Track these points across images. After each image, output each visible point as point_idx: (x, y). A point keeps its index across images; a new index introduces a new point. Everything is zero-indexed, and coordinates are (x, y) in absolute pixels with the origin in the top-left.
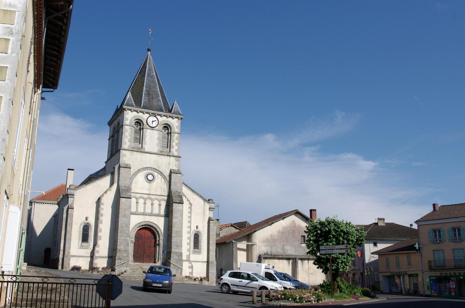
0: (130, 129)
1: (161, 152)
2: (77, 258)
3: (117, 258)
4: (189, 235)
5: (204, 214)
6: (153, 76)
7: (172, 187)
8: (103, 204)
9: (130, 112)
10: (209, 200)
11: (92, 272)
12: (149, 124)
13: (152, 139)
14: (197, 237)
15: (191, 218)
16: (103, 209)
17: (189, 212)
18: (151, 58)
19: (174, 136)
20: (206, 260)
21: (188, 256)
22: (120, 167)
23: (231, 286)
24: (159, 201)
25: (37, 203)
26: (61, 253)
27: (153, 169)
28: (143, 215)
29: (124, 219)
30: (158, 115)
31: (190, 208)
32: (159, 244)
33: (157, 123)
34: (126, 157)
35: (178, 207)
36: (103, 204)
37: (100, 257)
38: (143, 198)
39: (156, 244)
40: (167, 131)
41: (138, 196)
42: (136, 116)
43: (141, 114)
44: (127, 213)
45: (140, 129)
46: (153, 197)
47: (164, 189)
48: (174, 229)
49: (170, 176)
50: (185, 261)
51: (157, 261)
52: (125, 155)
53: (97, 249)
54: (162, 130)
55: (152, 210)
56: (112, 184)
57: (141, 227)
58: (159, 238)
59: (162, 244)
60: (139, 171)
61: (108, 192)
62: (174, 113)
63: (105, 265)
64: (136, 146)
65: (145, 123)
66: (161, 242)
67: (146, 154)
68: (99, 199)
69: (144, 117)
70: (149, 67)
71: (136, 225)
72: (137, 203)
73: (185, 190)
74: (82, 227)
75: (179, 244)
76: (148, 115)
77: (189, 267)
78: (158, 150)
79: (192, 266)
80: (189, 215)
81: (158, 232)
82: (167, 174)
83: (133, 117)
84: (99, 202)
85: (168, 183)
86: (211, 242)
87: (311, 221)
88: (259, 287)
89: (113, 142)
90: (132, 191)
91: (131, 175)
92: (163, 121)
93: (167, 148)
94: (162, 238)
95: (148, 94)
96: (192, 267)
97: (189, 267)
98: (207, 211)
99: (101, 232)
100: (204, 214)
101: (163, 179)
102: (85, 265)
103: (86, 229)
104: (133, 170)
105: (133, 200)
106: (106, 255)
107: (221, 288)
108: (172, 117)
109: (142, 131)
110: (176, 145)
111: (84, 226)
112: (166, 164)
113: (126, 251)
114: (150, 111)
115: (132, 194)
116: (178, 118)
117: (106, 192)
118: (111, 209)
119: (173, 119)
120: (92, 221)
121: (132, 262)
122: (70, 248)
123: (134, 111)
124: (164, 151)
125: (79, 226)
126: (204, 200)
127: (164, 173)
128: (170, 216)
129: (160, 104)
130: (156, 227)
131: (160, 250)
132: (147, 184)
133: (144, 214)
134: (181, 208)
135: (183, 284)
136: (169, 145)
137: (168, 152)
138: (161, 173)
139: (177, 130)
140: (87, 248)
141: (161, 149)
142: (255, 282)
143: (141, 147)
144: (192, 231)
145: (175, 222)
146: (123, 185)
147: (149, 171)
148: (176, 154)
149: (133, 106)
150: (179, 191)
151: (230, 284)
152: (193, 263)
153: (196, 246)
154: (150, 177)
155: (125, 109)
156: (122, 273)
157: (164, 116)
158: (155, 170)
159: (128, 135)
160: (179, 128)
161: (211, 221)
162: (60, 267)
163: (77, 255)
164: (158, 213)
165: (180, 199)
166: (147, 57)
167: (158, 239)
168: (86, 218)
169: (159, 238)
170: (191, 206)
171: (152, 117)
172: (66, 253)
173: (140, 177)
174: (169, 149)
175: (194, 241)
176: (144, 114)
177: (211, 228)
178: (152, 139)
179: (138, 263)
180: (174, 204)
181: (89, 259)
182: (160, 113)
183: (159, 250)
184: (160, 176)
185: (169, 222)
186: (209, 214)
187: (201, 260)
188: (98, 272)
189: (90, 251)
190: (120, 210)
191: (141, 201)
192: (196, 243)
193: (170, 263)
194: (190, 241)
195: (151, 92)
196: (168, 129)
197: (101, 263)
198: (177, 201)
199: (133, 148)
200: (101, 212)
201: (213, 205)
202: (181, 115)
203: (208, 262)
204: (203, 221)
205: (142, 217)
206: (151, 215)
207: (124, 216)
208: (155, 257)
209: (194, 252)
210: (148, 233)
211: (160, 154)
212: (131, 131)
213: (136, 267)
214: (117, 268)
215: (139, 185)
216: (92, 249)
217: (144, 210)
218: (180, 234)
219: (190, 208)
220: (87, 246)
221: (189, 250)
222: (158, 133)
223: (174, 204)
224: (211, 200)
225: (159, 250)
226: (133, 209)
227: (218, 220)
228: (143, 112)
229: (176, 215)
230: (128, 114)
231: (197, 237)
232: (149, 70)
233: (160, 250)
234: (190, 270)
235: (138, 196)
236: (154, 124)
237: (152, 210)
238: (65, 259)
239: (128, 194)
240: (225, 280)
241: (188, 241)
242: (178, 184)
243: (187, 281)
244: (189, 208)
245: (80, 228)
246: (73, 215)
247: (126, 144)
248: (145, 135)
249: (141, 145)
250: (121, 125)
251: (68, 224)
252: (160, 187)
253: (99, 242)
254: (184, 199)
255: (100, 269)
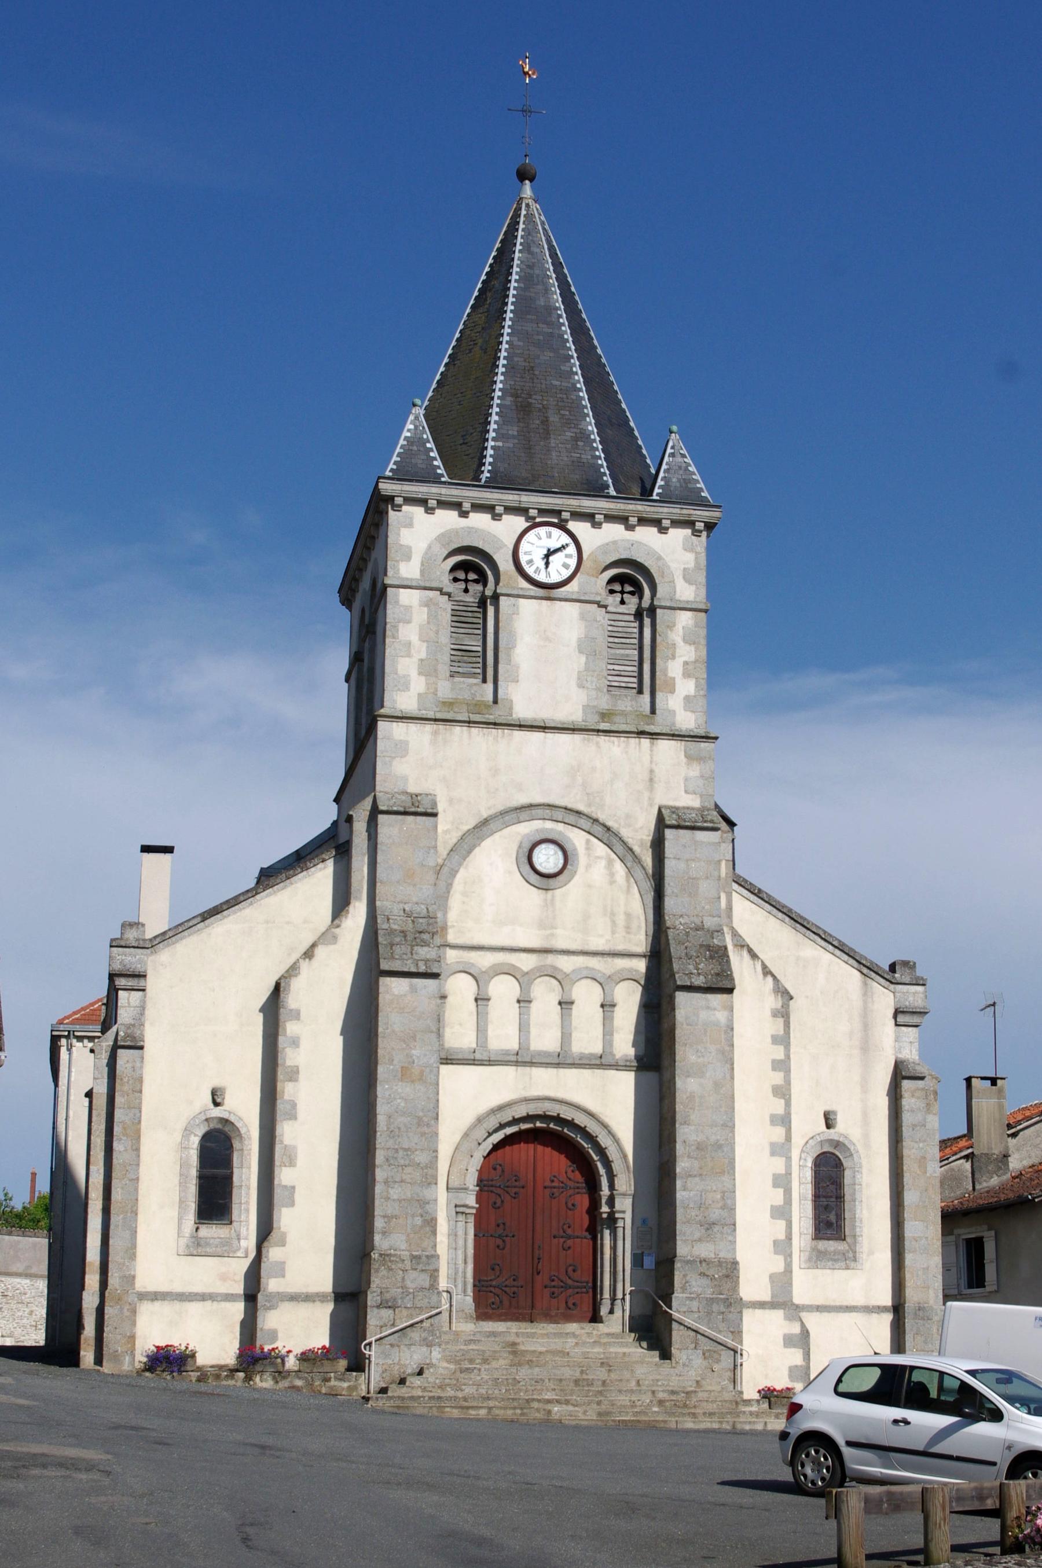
0: (427, 604)
1: (604, 716)
2: (177, 1305)
3: (372, 1298)
4: (778, 1165)
5: (866, 1047)
6: (551, 309)
7: (670, 904)
8: (296, 1015)
9: (418, 511)
10: (893, 968)
11: (248, 1378)
12: (530, 571)
13: (551, 649)
14: (830, 1177)
15: (787, 1072)
16: (295, 1043)
17: (776, 1040)
18: (539, 218)
19: (671, 626)
20: (887, 1300)
21: (782, 1282)
22: (375, 812)
23: (846, 1451)
24: (604, 982)
25: (80, 1039)
26: (92, 1280)
27: (559, 815)
28: (517, 1063)
29: (405, 1089)
30: (578, 516)
31: (783, 1014)
32: (612, 1221)
33: (573, 563)
34: (409, 756)
35: (703, 1015)
36: (296, 1015)
37: (294, 1298)
38: (510, 971)
39: (597, 1222)
40: (632, 602)
41: (484, 961)
42: (456, 532)
43: (480, 520)
44: (422, 1054)
45: (482, 603)
46: (566, 964)
47: (628, 915)
48: (686, 1135)
49: (658, 845)
50: (761, 1305)
51: (604, 1311)
52: (402, 749)
53: (273, 1254)
54: (602, 595)
55: (566, 1037)
56: (341, 902)
57: (509, 1130)
58: (612, 1186)
59: (628, 1216)
60: (483, 827)
61: (320, 951)
62: (664, 500)
63: (320, 1338)
64: (466, 695)
65: (505, 564)
66: (624, 1206)
67: (518, 734)
68: (277, 988)
69: (497, 533)
70: (528, 267)
71: (480, 1120)
72: (481, 999)
73: (748, 917)
74: (195, 1141)
75: (715, 1214)
76: (519, 523)
77: (789, 1341)
78: (585, 708)
79: (805, 1334)
80: (779, 1053)
81: (602, 1152)
82: (639, 832)
83: (440, 538)
84: (273, 1008)
85: (648, 886)
86: (910, 1197)
87: (288, 923)
88: (1010, 1457)
89: (359, 688)
90: (452, 937)
91: (443, 851)
92: (605, 548)
93: (640, 691)
94: (625, 1183)
95: (521, 406)
96: (802, 1340)
97: (789, 1341)
98: (886, 1030)
99: (292, 1163)
100: (866, 1047)
101: (619, 866)
102: (213, 1341)
103: (216, 1150)
104: (449, 827)
105: (460, 989)
106: (326, 1284)
107: (792, 1463)
108: (656, 523)
109: (491, 610)
110: (686, 675)
111: (207, 1138)
112: (639, 780)
113: (426, 1262)
114: (527, 499)
115: (451, 955)
116: (690, 524)
117: (309, 954)
118: (339, 1041)
119: (663, 530)
120: (244, 1108)
121: (467, 1318)
122: (133, 1257)
123: (443, 504)
124: (624, 714)
125: (178, 1137)
126: (867, 967)
127: (625, 833)
128: (666, 1063)
129: (586, 457)
130: (592, 1127)
131: (619, 1249)
132: (532, 898)
133: (522, 1059)
134: (721, 1016)
135: (735, 1432)
136: (646, 677)
137: (640, 716)
138: (608, 835)
139: (687, 592)
140: (224, 1251)
141: (604, 703)
142: (983, 1428)
143: (490, 697)
144: (798, 1141)
145: (691, 1097)
146: (396, 910)
147: (537, 824)
148: (687, 721)
149: (436, 480)
150: (709, 923)
151: (841, 1442)
152: (812, 1320)
153: (829, 1225)
154: (547, 859)
155: (391, 499)
156: (402, 1381)
157: (610, 518)
158: (571, 818)
159: (414, 638)
160: (702, 578)
161: (906, 1084)
162: (87, 1356)
163: (178, 1287)
164: (597, 1048)
165: (714, 967)
166: (517, 215)
167: (605, 1191)
168: (214, 1093)
169: (612, 1186)
170: (786, 1006)
171: (542, 531)
172: (113, 1281)
173: (494, 862)
174: (646, 697)
175: (817, 1197)
176: (496, 517)
177: (907, 1119)
178: (551, 649)
179: (500, 1326)
180: (681, 997)
181: (238, 1309)
182: (588, 504)
183: (614, 1248)
184: (601, 849)
185: (661, 1099)
186: (892, 1045)
187: (860, 1301)
188: (280, 1374)
189: (243, 1265)
190: (381, 1043)
191: (503, 991)
192: (827, 1208)
193: (670, 1319)
194: (788, 1193)
195: (535, 400)
196: (638, 591)
197: (301, 1329)
198: (699, 981)
199: (449, 704)
200: (290, 1057)
201: (913, 996)
202: (704, 504)
203: (898, 1309)
204: (865, 1086)
205: (509, 1072)
206: (561, 1060)
207: (405, 1074)
208: (595, 1288)
209: (817, 1259)
210: (553, 1163)
211: (598, 727)
212: (432, 617)
213: (488, 1346)
214: (373, 1353)
215: (488, 901)
216: (252, 1254)
217: (524, 1032)
218: (721, 1158)
219: (783, 1014)
220: (226, 1243)
221: (783, 1247)
222: (583, 617)
223: (681, 997)
224: (906, 964)
225: (614, 1248)
226: (460, 1035)
227: (994, 1081)
228: (488, 508)
229: (693, 1058)
230: (410, 525)
231: (830, 1177)
232: (526, 279)
233: (619, 1249)
234: (796, 1357)
235: (484, 961)
236: (557, 571)
237: (566, 1037)
238: (108, 1310)
239: (423, 952)
240: (815, 1414)
241: (777, 1197)
242: (705, 888)
243: (757, 1415)
244: (775, 1014)
245: (183, 1147)
246: (140, 1080)
247: (406, 687)
248: (512, 635)
249: (489, 687)
250: (379, 585)
251: (117, 1129)
252: (603, 908)
253: (285, 1218)
254: (741, 966)
255: (291, 1363)
